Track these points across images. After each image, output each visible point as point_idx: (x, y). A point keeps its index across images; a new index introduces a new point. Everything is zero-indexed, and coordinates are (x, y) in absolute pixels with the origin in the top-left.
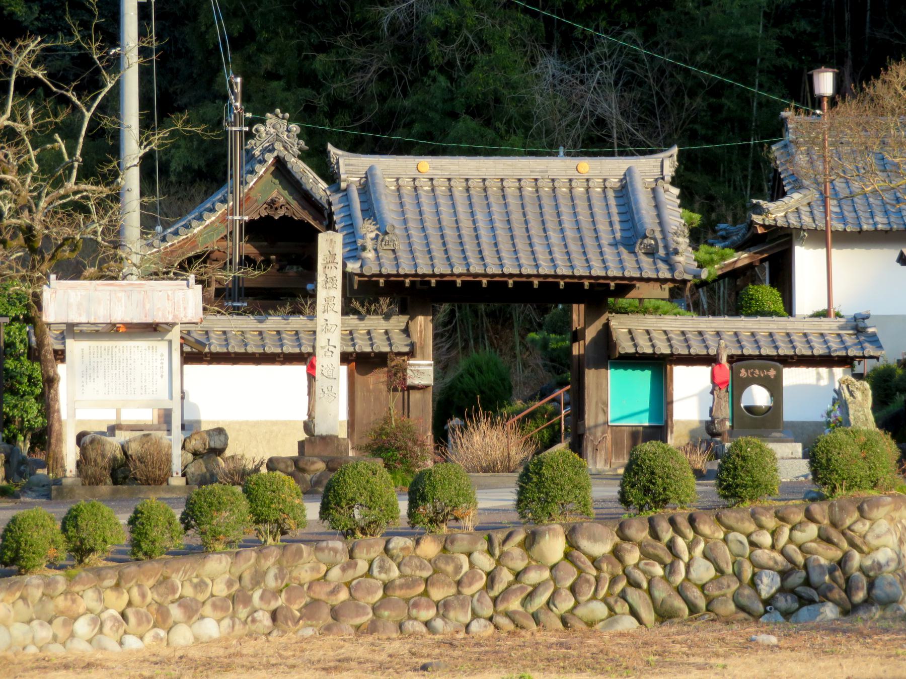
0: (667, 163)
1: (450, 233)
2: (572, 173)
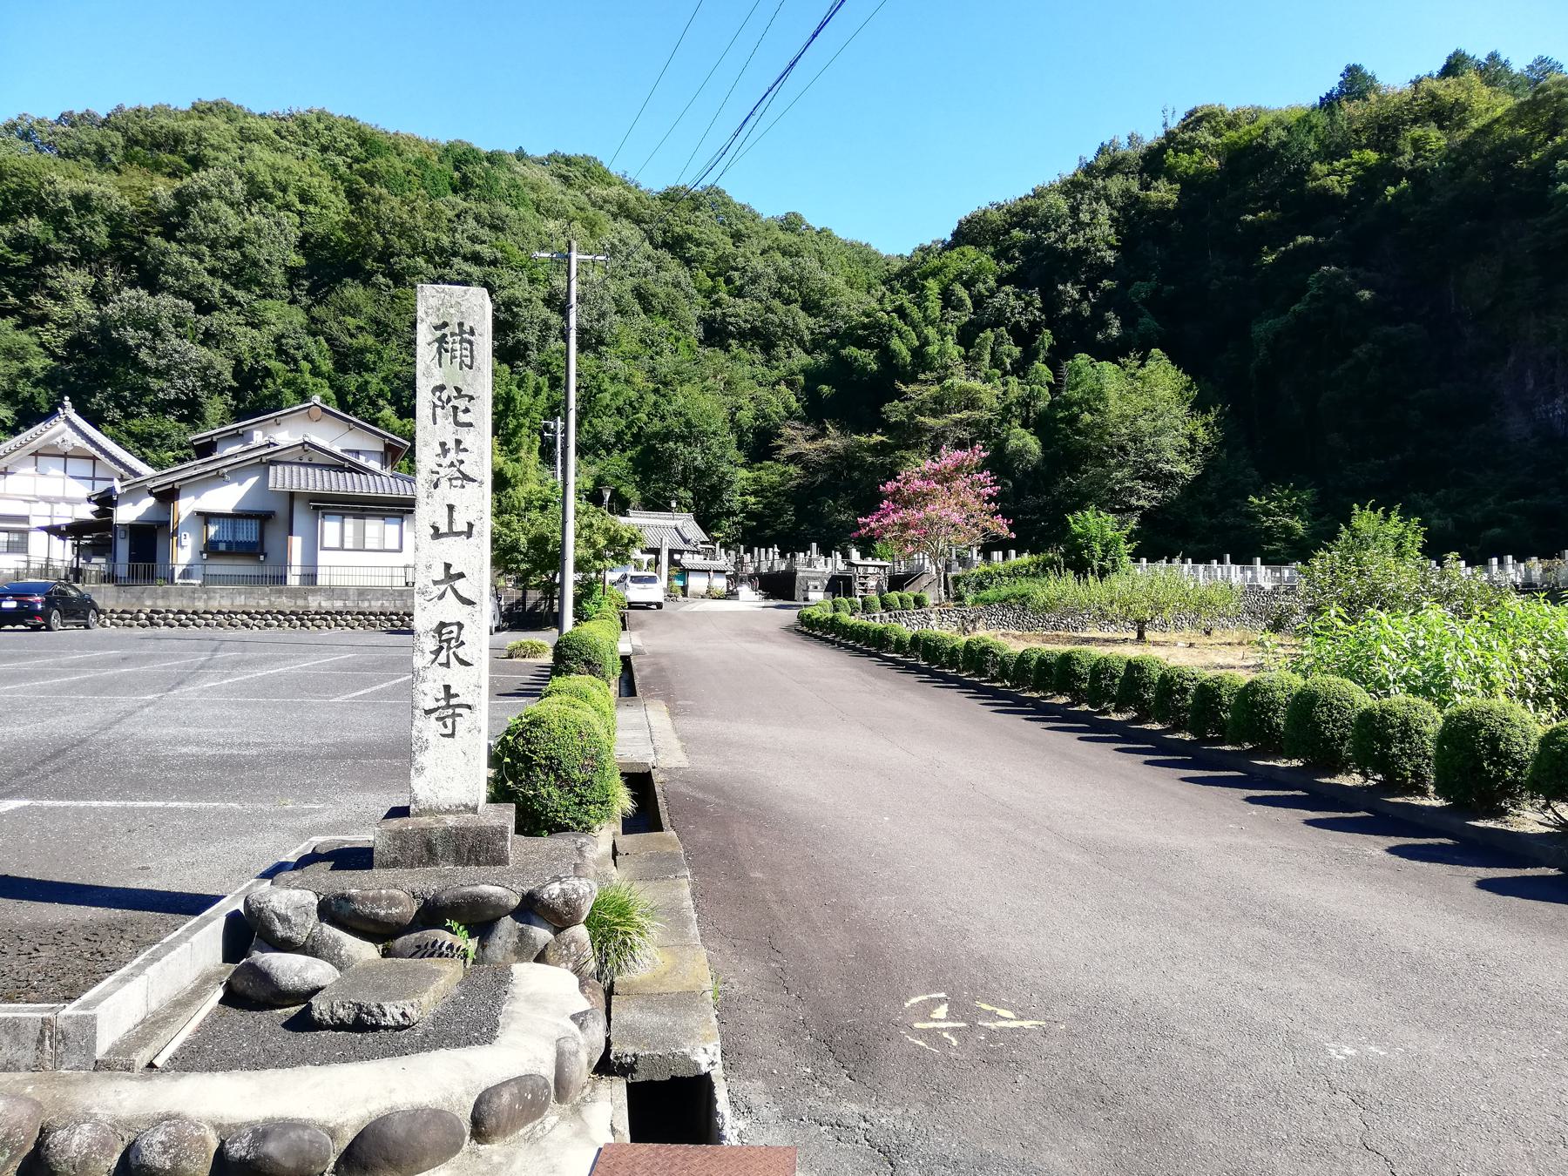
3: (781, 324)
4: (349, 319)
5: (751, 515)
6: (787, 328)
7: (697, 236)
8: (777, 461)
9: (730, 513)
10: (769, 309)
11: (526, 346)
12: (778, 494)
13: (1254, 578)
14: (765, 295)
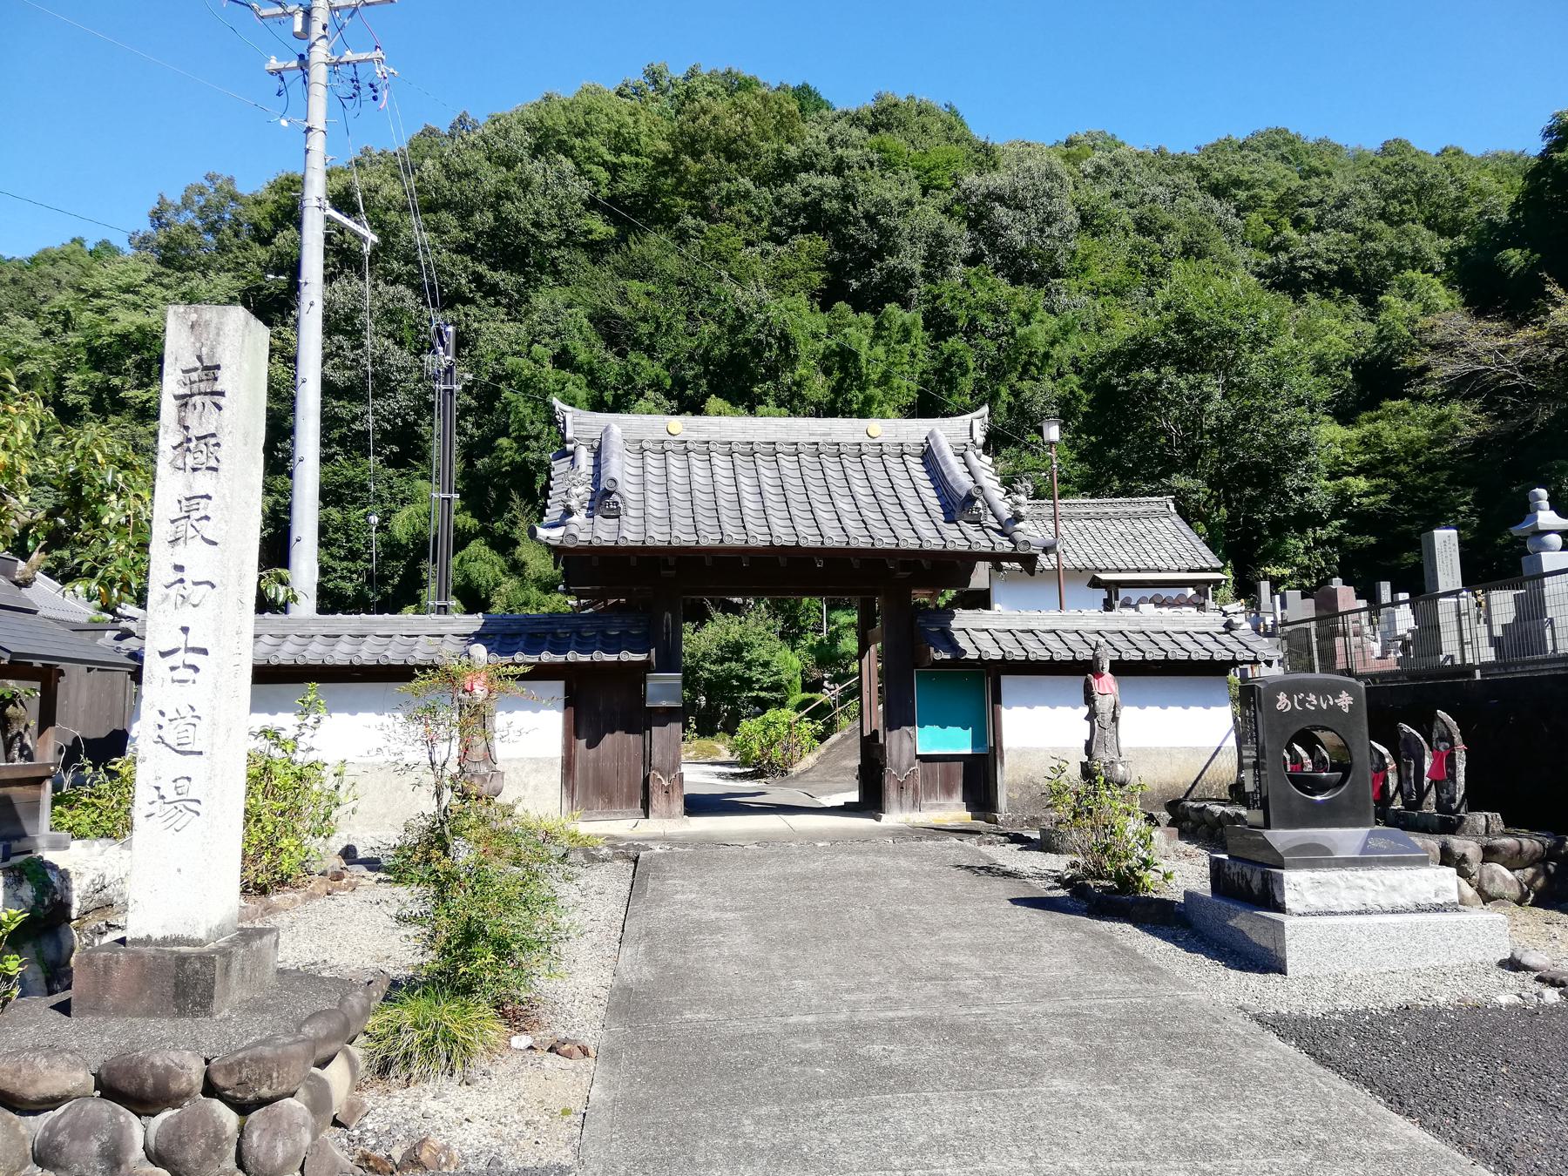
0: (977, 424)
1: (702, 499)
2: (860, 437)
3: (1391, 252)
4: (635, 285)
5: (1361, 521)
6: (1401, 256)
7: (1246, 177)
8: (1417, 399)
9: (1306, 519)
10: (1368, 236)
11: (907, 279)
12: (1430, 467)
13: (1428, 629)
14: (1359, 221)
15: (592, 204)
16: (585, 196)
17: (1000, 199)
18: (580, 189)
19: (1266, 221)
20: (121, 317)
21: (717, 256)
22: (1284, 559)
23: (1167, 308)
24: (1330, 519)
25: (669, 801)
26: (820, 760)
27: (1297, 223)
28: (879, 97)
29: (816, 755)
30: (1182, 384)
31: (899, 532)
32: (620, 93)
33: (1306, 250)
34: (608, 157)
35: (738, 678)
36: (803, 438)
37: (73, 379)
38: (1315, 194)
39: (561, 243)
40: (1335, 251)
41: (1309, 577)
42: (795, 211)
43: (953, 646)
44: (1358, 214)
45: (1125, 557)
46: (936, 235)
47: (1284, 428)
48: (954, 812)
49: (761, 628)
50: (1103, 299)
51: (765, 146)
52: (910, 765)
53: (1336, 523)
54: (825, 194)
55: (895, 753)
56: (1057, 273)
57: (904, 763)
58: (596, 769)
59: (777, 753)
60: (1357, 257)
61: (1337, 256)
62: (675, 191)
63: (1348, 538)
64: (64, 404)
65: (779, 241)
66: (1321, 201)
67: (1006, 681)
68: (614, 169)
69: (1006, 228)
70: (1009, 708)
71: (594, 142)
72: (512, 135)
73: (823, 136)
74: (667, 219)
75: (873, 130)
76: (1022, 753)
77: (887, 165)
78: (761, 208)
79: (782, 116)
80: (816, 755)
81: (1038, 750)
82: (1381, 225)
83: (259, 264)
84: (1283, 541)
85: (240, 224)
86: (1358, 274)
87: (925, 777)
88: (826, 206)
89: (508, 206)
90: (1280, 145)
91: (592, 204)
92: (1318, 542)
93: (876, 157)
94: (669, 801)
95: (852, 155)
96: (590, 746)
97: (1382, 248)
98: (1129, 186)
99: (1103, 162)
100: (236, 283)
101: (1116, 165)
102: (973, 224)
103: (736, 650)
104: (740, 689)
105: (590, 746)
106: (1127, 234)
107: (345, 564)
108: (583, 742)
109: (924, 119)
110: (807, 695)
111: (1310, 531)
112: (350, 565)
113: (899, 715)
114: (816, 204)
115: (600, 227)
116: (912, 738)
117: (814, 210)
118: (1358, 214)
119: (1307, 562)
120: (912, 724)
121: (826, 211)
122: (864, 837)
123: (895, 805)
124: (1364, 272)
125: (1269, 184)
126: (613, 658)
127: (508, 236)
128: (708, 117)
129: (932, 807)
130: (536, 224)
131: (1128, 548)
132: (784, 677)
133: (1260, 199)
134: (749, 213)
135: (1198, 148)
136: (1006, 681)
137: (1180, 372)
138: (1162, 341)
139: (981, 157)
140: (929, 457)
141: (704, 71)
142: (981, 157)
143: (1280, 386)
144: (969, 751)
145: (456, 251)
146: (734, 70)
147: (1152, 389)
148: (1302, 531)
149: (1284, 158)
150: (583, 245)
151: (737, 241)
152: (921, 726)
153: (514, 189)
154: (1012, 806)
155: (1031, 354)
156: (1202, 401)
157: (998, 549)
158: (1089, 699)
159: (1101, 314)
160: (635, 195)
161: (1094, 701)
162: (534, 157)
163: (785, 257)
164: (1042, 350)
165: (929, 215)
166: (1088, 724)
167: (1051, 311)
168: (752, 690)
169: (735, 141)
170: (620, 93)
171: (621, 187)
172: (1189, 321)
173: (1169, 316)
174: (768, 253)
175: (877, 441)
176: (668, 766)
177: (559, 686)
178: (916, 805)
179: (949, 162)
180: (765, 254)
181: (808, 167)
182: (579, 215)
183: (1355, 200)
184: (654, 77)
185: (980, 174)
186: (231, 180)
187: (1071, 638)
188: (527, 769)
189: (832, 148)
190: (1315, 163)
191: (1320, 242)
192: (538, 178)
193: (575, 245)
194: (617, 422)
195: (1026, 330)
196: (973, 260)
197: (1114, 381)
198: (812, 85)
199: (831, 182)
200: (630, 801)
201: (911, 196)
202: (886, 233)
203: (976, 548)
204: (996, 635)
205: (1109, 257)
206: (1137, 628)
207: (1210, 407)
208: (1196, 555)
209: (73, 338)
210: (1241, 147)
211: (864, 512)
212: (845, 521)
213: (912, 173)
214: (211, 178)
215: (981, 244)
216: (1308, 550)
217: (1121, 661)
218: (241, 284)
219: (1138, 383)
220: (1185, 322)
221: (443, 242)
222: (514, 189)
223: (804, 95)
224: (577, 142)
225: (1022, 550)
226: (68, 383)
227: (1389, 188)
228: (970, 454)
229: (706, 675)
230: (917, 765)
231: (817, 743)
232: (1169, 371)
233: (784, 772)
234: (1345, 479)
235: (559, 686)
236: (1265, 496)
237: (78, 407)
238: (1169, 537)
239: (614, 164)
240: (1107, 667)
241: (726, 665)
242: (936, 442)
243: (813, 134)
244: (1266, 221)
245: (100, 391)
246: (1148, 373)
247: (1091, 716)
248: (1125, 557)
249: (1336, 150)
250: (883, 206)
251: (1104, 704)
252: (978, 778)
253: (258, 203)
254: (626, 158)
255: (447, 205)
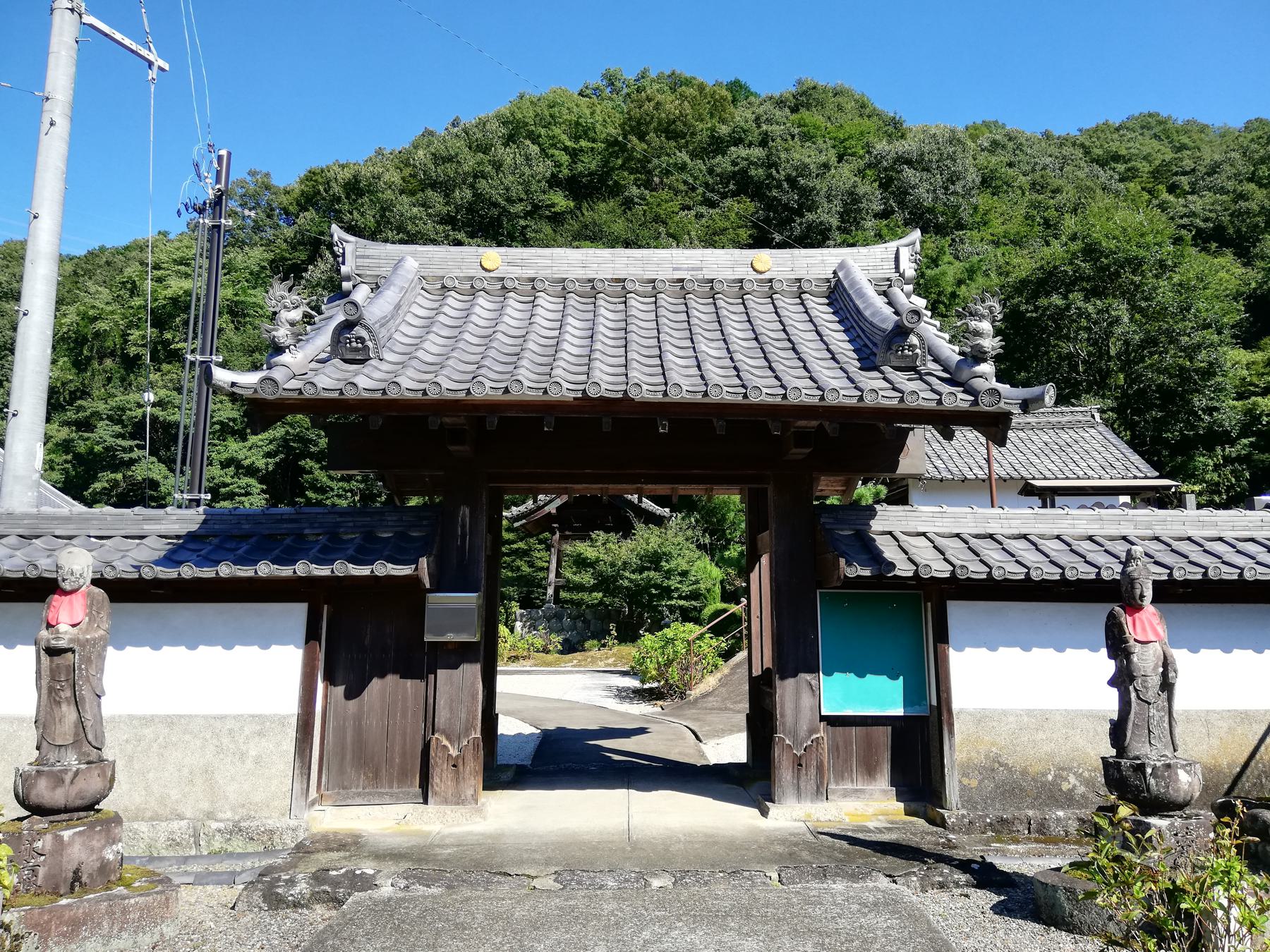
0: (905, 254)
7: (1123, 152)
9: (1215, 438)
10: (1242, 196)
14: (1230, 185)
15: (554, 182)
16: (548, 174)
17: (909, 162)
18: (544, 168)
19: (1143, 189)
20: (172, 283)
21: (657, 219)
22: (1193, 476)
23: (1074, 238)
24: (1239, 437)
25: (457, 779)
26: (723, 682)
27: (1172, 189)
28: (799, 82)
29: (719, 675)
30: (1091, 309)
31: (786, 379)
32: (581, 94)
33: (1184, 210)
34: (568, 143)
35: (657, 586)
36: (665, 274)
37: (135, 334)
38: (1188, 164)
39: (527, 214)
40: (1210, 211)
41: (1220, 494)
42: (725, 178)
43: (873, 556)
44: (1229, 178)
45: (1051, 466)
46: (851, 194)
47: (1191, 352)
48: (873, 806)
49: (680, 539)
50: (1002, 249)
51: (700, 126)
52: (813, 731)
53: (1245, 441)
54: (752, 163)
55: (789, 712)
56: (960, 226)
57: (804, 727)
58: (359, 730)
59: (674, 673)
60: (1231, 215)
61: (1213, 215)
62: (622, 167)
63: (1258, 456)
64: (127, 355)
65: (712, 205)
66: (1193, 170)
67: (958, 612)
68: (574, 154)
69: (914, 187)
70: (960, 649)
71: (557, 131)
72: (488, 127)
73: (751, 117)
74: (616, 190)
75: (794, 110)
76: (982, 718)
77: (807, 137)
78: (696, 178)
79: (716, 100)
80: (719, 675)
81: (1005, 713)
82: (1252, 186)
83: (285, 241)
84: (1192, 458)
85: (273, 209)
86: (1231, 231)
87: (835, 749)
88: (753, 172)
89: (482, 184)
90: (1154, 126)
91: (554, 182)
92: (1228, 460)
93: (796, 131)
94: (457, 779)
95: (776, 129)
96: (349, 695)
97: (1254, 206)
98: (1022, 157)
99: (998, 137)
100: (266, 255)
101: (1010, 139)
102: (885, 185)
103: (654, 560)
104: (660, 597)
105: (349, 695)
106: (1023, 194)
107: (341, 484)
108: (340, 690)
109: (839, 99)
110: (725, 606)
111: (1219, 450)
112: (345, 485)
113: (797, 654)
114: (744, 172)
115: (560, 201)
116: (815, 691)
117: (743, 178)
118: (1229, 178)
119: (1216, 478)
120: (814, 670)
121: (752, 177)
122: (733, 861)
123: (790, 791)
124: (1238, 231)
125: (1145, 158)
126: (364, 571)
127: (483, 208)
128: (652, 104)
129: (846, 794)
130: (509, 200)
131: (1054, 458)
132: (702, 586)
133: (1137, 170)
134: (685, 182)
135: (1080, 130)
136: (958, 612)
137: (1086, 299)
138: (1069, 269)
139: (891, 129)
140: (838, 294)
141: (653, 74)
142: (891, 129)
143: (1188, 310)
144: (899, 711)
145: (441, 223)
146: (678, 72)
147: (1061, 313)
148: (1210, 449)
149: (1156, 136)
150: (547, 217)
151: (675, 205)
152: (828, 673)
153: (489, 169)
154: (968, 800)
155: (940, 294)
156: (1111, 324)
157: (948, 403)
158: (1117, 645)
159: (1001, 261)
160: (591, 174)
161: (1128, 654)
162: (506, 145)
163: (717, 218)
164: (950, 290)
165: (844, 176)
166: (1114, 693)
167: (957, 258)
168: (671, 598)
169: (674, 122)
170: (581, 94)
171: (580, 167)
172: (1095, 250)
173: (1076, 246)
174: (702, 216)
175: (767, 276)
176: (458, 727)
177: (299, 611)
178: (821, 792)
179: (862, 133)
180: (699, 216)
181: (738, 142)
182: (544, 192)
183: (1226, 167)
184: (611, 80)
185: (889, 143)
186: (267, 175)
187: (1052, 546)
188: (247, 731)
189: (759, 127)
190: (1185, 140)
191: (1197, 203)
192: (509, 161)
193: (541, 217)
194: (414, 255)
195: (937, 271)
196: (885, 214)
197: (1023, 308)
198: (743, 80)
199: (757, 153)
200: (403, 777)
201: (829, 160)
202: (806, 192)
203: (911, 403)
204: (940, 541)
205: (1007, 213)
206: (1149, 533)
207: (1118, 330)
208: (1128, 464)
209: (137, 302)
210: (1118, 130)
211: (737, 356)
212: (707, 366)
213: (830, 143)
214: (252, 173)
215: (891, 202)
216: (1217, 467)
217: (1171, 581)
218: (270, 256)
219: (1047, 308)
220: (1091, 251)
221: (429, 215)
222: (489, 169)
223: (737, 89)
224: (543, 131)
225: (986, 405)
226: (131, 338)
227: (1256, 156)
228: (896, 291)
229: (626, 583)
230: (822, 732)
231: (720, 662)
232: (1077, 297)
233: (682, 695)
234: (1253, 398)
235: (299, 611)
236: (1174, 416)
237: (138, 357)
238: (1097, 446)
239: (574, 149)
240: (1149, 594)
241: (645, 574)
242: (847, 275)
243: (742, 115)
244: (1143, 189)
245: (156, 344)
246: (1056, 300)
247: (1123, 679)
248: (1051, 466)
249: (1203, 129)
250: (803, 169)
251: (1146, 660)
252: (914, 752)
253: (287, 193)
254: (583, 143)
255: (434, 185)
